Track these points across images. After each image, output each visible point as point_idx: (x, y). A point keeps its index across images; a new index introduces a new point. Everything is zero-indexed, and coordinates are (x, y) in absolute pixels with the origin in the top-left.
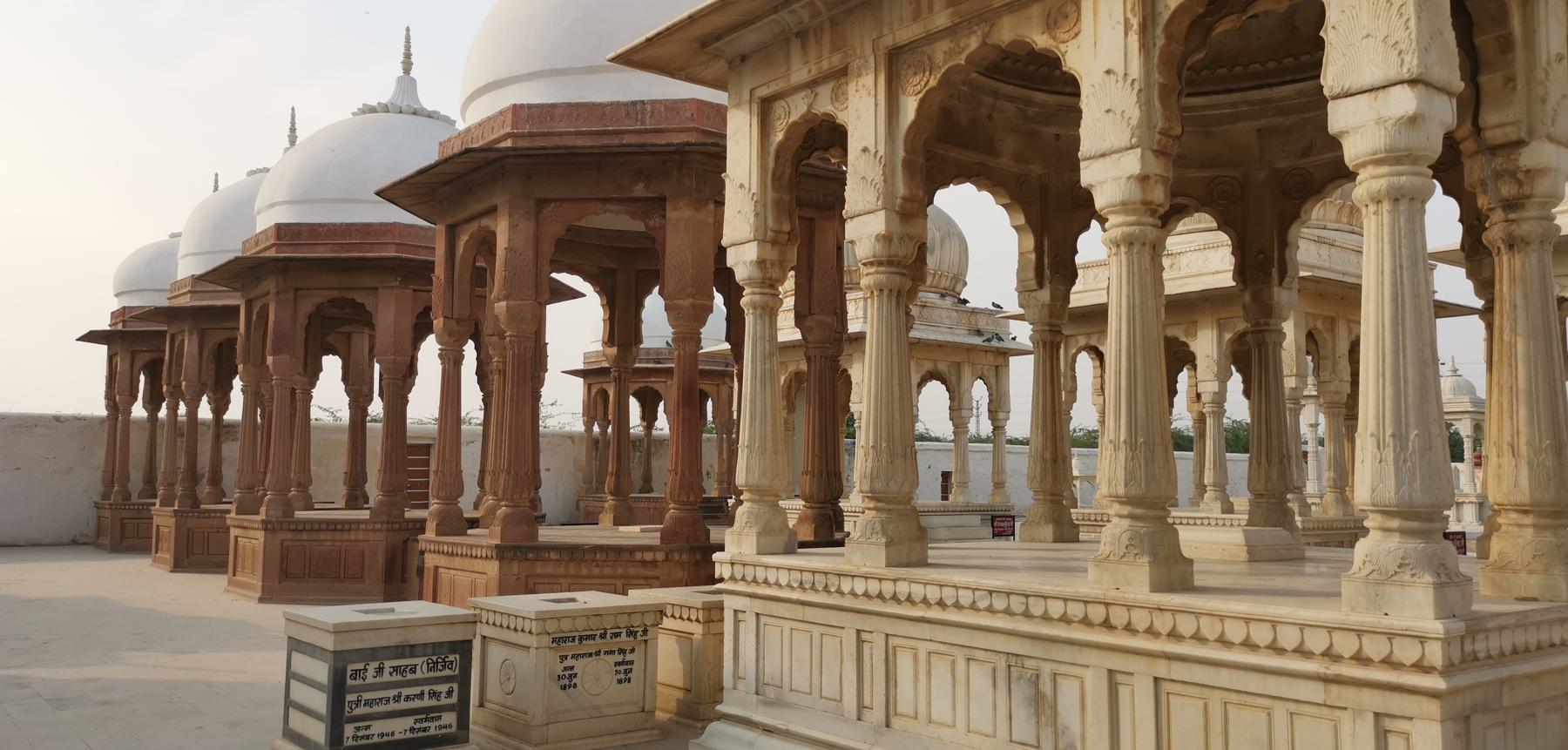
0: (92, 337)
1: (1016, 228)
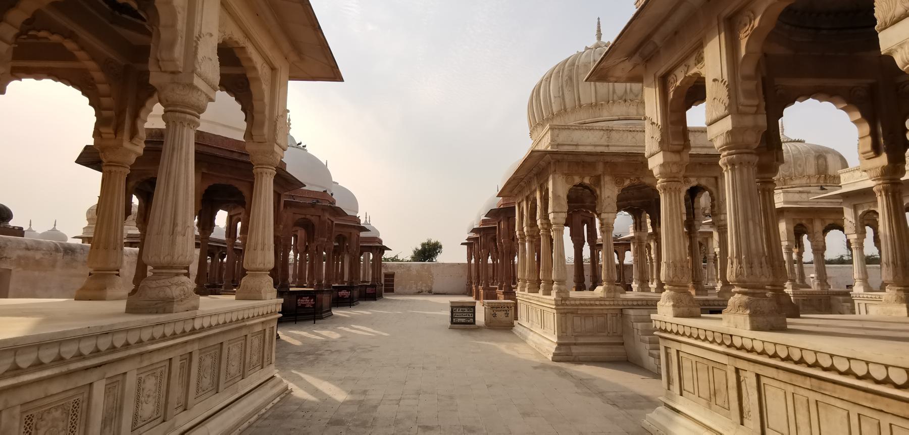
0: (462, 244)
1: (855, 122)
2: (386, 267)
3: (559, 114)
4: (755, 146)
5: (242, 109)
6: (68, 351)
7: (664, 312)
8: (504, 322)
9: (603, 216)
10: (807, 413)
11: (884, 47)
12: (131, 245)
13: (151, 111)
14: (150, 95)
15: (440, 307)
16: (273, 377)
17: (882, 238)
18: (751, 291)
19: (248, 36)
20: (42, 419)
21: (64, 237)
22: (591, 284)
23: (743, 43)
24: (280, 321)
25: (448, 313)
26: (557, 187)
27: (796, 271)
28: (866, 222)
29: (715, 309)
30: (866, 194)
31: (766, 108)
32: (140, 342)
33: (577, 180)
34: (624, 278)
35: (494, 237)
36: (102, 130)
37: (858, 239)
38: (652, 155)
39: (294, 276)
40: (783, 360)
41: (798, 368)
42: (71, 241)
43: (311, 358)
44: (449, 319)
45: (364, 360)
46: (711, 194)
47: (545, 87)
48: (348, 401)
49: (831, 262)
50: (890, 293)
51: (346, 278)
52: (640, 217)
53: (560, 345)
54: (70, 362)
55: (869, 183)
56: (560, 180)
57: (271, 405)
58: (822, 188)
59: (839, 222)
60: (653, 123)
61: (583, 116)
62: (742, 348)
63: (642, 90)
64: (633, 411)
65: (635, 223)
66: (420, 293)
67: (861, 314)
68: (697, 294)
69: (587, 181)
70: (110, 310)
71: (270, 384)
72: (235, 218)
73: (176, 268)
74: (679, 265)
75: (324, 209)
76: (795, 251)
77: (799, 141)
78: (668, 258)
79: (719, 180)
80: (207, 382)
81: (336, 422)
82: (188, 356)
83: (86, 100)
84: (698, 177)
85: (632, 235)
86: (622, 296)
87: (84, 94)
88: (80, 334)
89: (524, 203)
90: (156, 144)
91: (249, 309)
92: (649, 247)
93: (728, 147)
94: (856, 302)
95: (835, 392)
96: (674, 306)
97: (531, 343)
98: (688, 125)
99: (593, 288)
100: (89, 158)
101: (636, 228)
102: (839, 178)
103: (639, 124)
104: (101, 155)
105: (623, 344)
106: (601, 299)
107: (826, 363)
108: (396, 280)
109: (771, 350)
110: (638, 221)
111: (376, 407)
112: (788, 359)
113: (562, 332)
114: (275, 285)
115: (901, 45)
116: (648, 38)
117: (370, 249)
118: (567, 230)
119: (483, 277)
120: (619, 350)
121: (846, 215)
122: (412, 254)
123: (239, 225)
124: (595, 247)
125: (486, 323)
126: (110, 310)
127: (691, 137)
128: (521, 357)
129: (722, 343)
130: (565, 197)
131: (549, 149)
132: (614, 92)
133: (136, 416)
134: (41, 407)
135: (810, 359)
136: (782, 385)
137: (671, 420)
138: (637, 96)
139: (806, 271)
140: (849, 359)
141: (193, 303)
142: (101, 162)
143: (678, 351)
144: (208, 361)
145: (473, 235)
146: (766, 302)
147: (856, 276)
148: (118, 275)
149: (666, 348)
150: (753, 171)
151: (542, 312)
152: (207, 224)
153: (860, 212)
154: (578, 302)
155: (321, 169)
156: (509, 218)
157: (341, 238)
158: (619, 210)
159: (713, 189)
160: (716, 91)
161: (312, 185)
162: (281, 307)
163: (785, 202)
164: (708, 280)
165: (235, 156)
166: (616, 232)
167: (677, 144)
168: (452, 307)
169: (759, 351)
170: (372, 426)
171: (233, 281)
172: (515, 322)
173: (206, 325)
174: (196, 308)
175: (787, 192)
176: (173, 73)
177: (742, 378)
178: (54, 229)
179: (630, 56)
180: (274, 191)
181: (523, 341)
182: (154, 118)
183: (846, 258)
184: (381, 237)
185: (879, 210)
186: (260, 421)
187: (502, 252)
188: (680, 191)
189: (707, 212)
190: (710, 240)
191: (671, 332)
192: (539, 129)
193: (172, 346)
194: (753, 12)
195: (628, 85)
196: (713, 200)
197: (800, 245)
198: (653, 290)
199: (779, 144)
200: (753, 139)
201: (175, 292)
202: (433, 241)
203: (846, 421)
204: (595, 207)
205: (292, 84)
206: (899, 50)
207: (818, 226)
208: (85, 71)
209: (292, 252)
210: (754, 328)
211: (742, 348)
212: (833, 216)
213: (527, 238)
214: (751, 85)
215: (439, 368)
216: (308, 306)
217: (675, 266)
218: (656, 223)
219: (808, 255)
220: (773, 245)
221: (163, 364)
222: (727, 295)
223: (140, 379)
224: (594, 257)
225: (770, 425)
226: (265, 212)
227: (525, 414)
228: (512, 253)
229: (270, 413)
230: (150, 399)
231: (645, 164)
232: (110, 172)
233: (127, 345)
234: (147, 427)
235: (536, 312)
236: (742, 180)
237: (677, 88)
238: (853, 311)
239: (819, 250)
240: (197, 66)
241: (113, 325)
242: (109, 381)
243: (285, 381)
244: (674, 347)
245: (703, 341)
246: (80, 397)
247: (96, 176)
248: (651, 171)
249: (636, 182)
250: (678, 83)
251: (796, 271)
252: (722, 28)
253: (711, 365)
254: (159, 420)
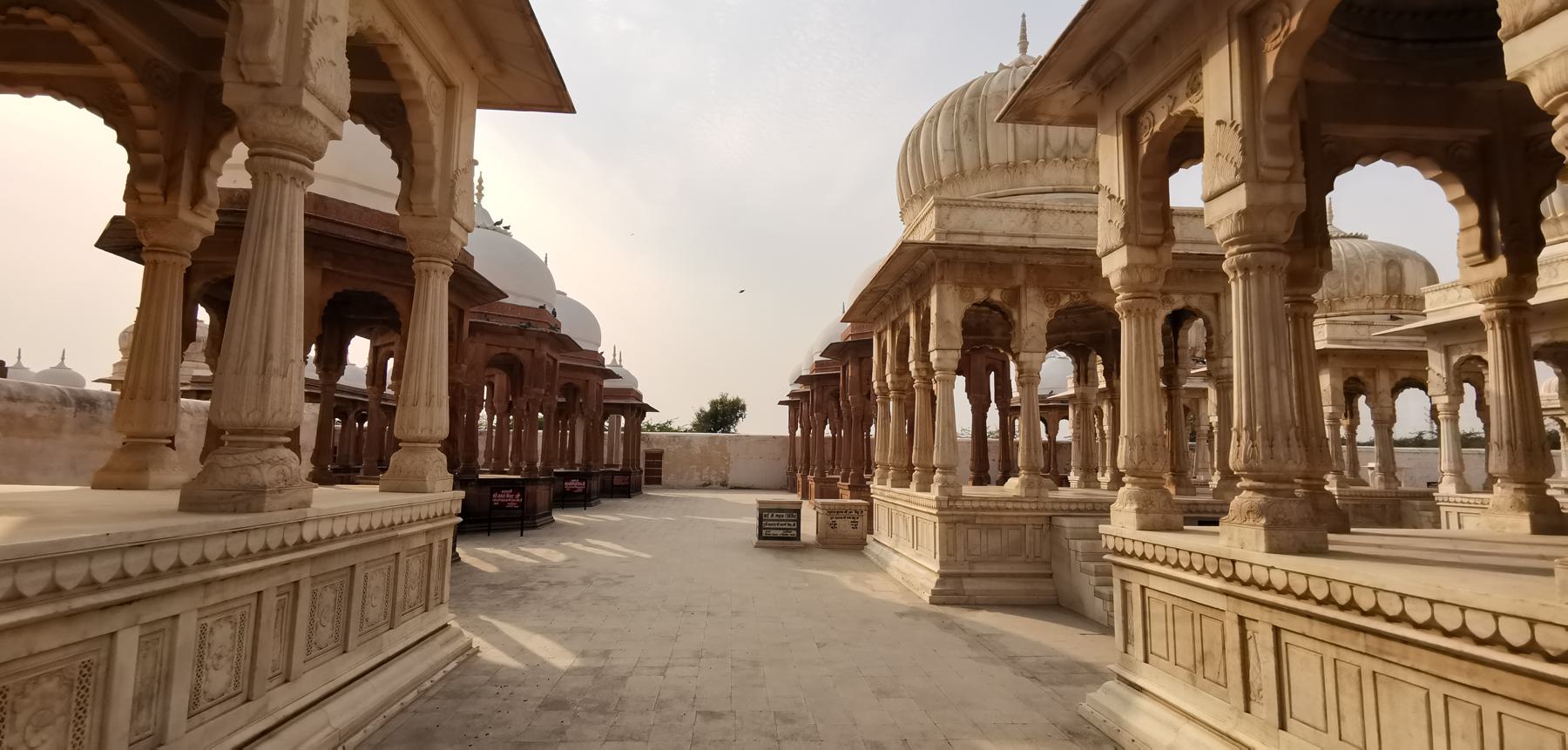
0: (781, 403)
1: (1455, 202)
2: (649, 440)
3: (951, 179)
4: (1285, 238)
5: (393, 157)
6: (70, 575)
7: (1123, 522)
8: (849, 537)
9: (1022, 357)
10: (1357, 693)
11: (1512, 68)
12: (199, 395)
13: (229, 156)
14: (228, 128)
15: (740, 510)
16: (446, 626)
17: (1491, 402)
18: (1270, 486)
19: (402, 25)
20: (23, 694)
21: (82, 381)
22: (999, 475)
23: (1271, 58)
24: (461, 531)
25: (755, 521)
26: (944, 306)
27: (1345, 456)
28: (1464, 377)
29: (1208, 518)
30: (1469, 328)
31: (1306, 174)
32: (204, 562)
33: (980, 295)
34: (1056, 466)
35: (835, 392)
36: (141, 188)
37: (1450, 404)
38: (1109, 252)
39: (488, 453)
40: (1320, 603)
41: (1346, 617)
42: (91, 387)
43: (514, 594)
44: (755, 531)
45: (604, 598)
46: (1207, 323)
47: (929, 130)
48: (575, 669)
49: (1403, 443)
50: (1502, 494)
51: (579, 458)
52: (1086, 361)
53: (943, 577)
54: (74, 594)
55: (1477, 310)
56: (951, 293)
57: (441, 674)
58: (1393, 318)
59: (1419, 375)
60: (1111, 197)
61: (993, 184)
62: (1251, 583)
63: (1096, 140)
64: (1064, 689)
65: (1078, 371)
66: (706, 486)
67: (1450, 527)
68: (1177, 494)
69: (996, 296)
70: (151, 507)
71: (440, 638)
72: (383, 351)
73: (270, 434)
74: (1149, 442)
75: (541, 337)
76: (1345, 422)
77: (1356, 237)
78: (1131, 430)
79: (1222, 300)
80: (325, 633)
81: (554, 704)
82: (291, 589)
83: (112, 134)
84: (1187, 294)
85: (1072, 392)
86: (1052, 495)
87: (107, 122)
88: (90, 545)
89: (888, 336)
90: (236, 212)
91: (402, 507)
92: (1100, 413)
93: (1239, 238)
94: (1443, 510)
95: (1406, 658)
96: (1138, 511)
97: (895, 574)
98: (1172, 204)
99: (1002, 481)
100: (119, 239)
101: (1077, 380)
102: (1422, 300)
103: (1088, 201)
104: (139, 232)
105: (1051, 576)
106: (1015, 500)
107: (1393, 607)
108: (665, 462)
109: (1299, 586)
110: (1082, 367)
111: (624, 678)
112: (1329, 601)
113: (948, 553)
114: (451, 468)
115: (1541, 65)
116: (1106, 48)
117: (622, 409)
118: (960, 381)
119: (815, 460)
120: (1044, 586)
121: (1431, 364)
122: (693, 418)
123: (391, 363)
124: (1008, 412)
125: (819, 539)
126: (151, 507)
127: (1179, 228)
128: (878, 596)
129: (1217, 575)
130: (959, 324)
131: (933, 239)
132: (1047, 143)
133: (196, 693)
134: (19, 673)
135: (1366, 602)
136: (1318, 646)
137: (1127, 703)
138: (1086, 151)
139: (1360, 457)
140: (1431, 602)
141: (301, 495)
142: (141, 246)
143: (1143, 588)
144: (329, 597)
145: (799, 388)
146: (1294, 506)
147: (1445, 466)
148: (172, 446)
149: (1123, 582)
150: (1279, 281)
151: (915, 520)
152: (333, 360)
153: (1455, 359)
154: (976, 505)
155: (536, 268)
156: (861, 359)
157: (571, 390)
158: (1049, 349)
159: (1211, 315)
160: (1221, 142)
161: (520, 296)
162: (459, 505)
163: (1331, 340)
164: (1198, 470)
165: (383, 242)
166: (1042, 389)
167: (1152, 232)
168: (761, 511)
169: (1280, 588)
170: (617, 711)
171: (380, 461)
172: (869, 538)
173: (324, 534)
174: (306, 504)
175: (1334, 323)
176: (264, 85)
177: (1249, 634)
178: (61, 366)
179: (1075, 78)
180: (450, 304)
181: (880, 568)
182: (233, 171)
183: (1427, 437)
184: (640, 389)
185: (1489, 356)
186: (420, 702)
187: (849, 417)
188: (1154, 316)
189: (1199, 354)
190: (1202, 403)
191: (1133, 555)
192: (917, 205)
193: (261, 570)
194: (1289, 5)
195: (1072, 129)
196: (1209, 333)
197: (1352, 413)
198: (1104, 486)
199: (1326, 239)
200: (1281, 226)
201: (268, 475)
202: (730, 398)
203: (1423, 707)
204: (1009, 342)
205: (484, 117)
206: (1537, 73)
207: (1384, 382)
208: (109, 83)
209: (483, 413)
210: (1273, 549)
211: (1251, 583)
212: (1410, 365)
213: (892, 394)
214: (1282, 132)
215: (736, 613)
216: (510, 505)
217: (1143, 443)
218: (1112, 371)
219: (1366, 431)
220: (1310, 410)
221: (246, 601)
222: (1227, 495)
223: (204, 627)
224: (1006, 430)
225: (1295, 714)
226: (433, 338)
227: (881, 693)
228: (866, 420)
229: (439, 687)
230: (223, 661)
231: (1096, 268)
232: (156, 263)
233: (179, 567)
234: (217, 710)
235: (905, 520)
236: (1260, 296)
237: (1155, 136)
238: (1436, 524)
239: (1385, 422)
240: (309, 75)
241: (151, 531)
242: (147, 630)
243: (467, 634)
244: (1137, 580)
245: (1186, 570)
246: (93, 657)
247: (129, 276)
248: (1107, 280)
249: (1081, 300)
250: (1157, 128)
251: (1345, 456)
252: (1235, 27)
253: (1198, 610)
254: (239, 699)
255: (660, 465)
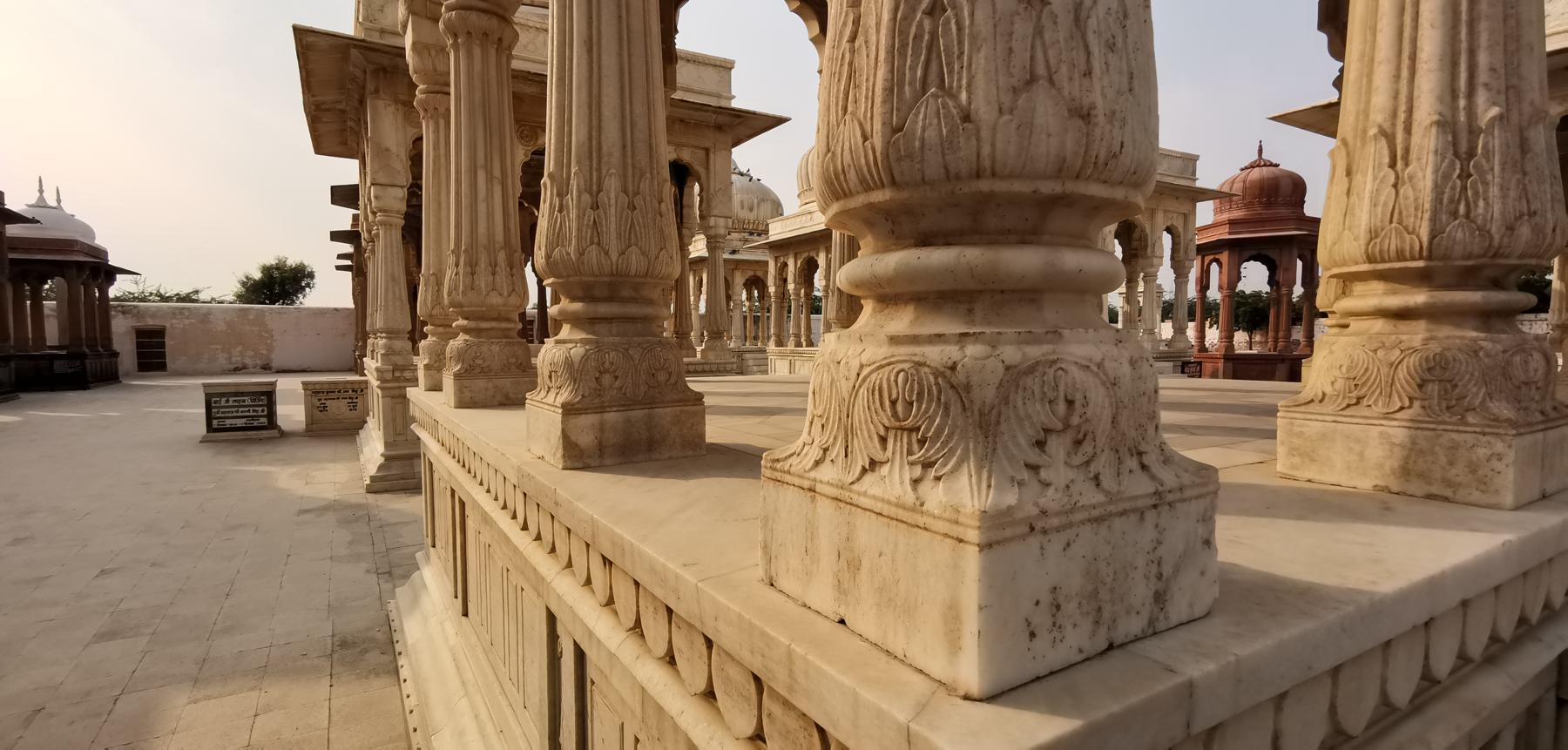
18: (472, 324)
53: (389, 459)
108: (169, 342)
122: (237, 288)
184: (100, 241)
202: (292, 262)
255: (163, 345)
